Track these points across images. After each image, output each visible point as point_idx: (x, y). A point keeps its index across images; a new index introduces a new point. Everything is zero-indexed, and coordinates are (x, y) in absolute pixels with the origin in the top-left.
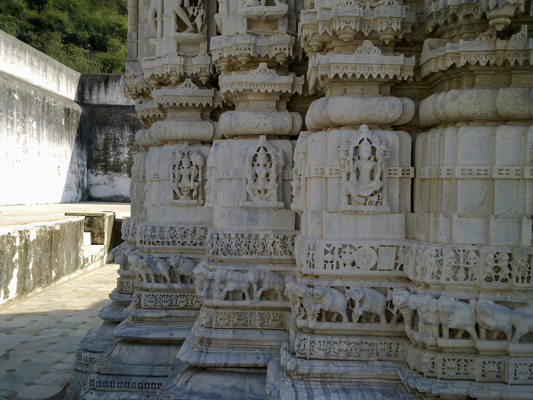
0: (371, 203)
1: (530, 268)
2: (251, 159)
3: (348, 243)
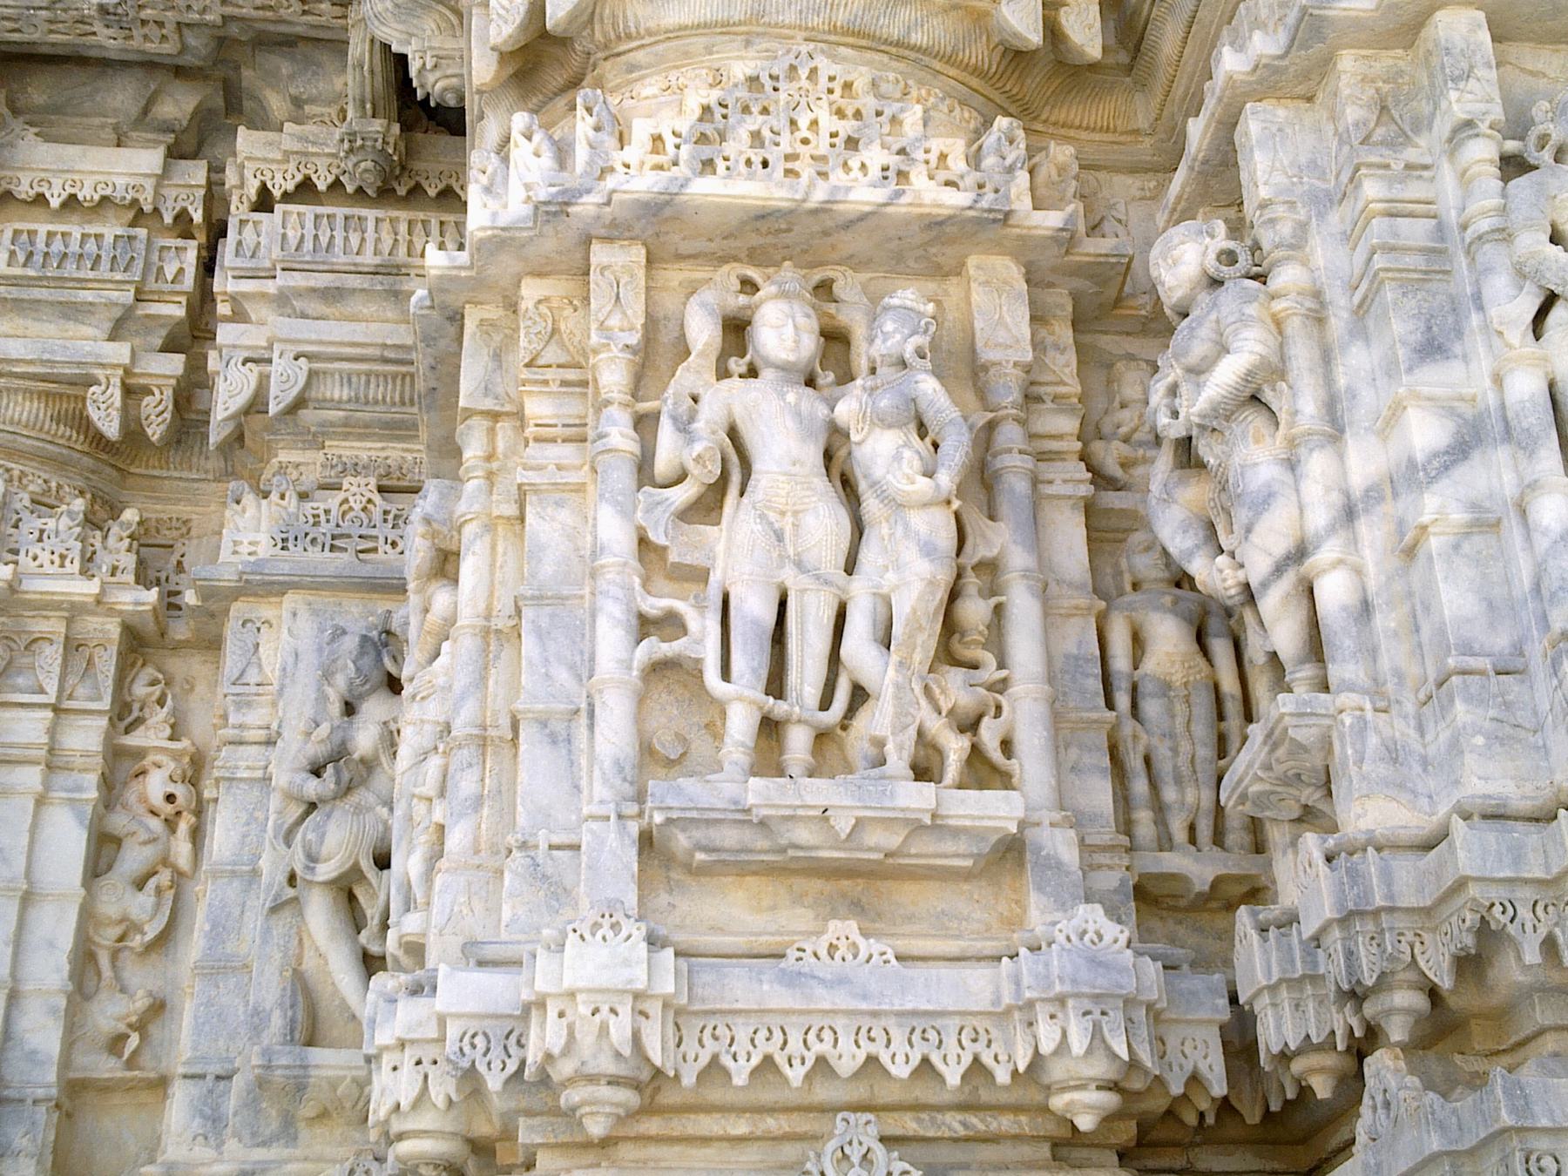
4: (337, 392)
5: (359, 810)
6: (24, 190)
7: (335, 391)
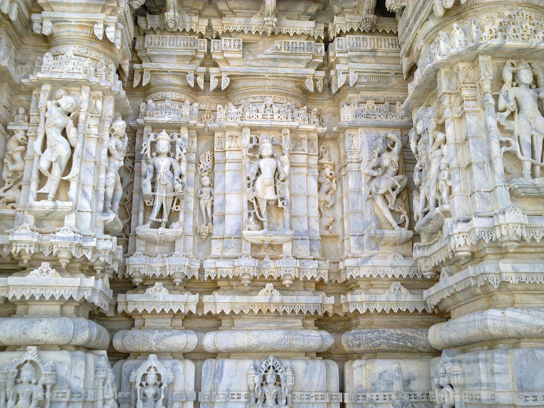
5: (387, 178)
6: (284, 32)
7: (364, 80)
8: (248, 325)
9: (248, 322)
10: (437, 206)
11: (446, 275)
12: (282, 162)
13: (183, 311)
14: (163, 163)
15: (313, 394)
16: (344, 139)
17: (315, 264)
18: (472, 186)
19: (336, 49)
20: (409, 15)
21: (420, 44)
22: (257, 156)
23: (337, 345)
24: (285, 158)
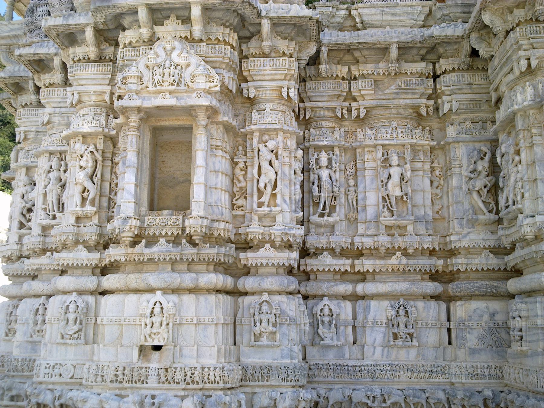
0: (74, 338)
1: (132, 375)
2: (35, 311)
3: (59, 362)
4: (463, 107)
5: (480, 179)
6: (403, 72)
8: (385, 279)
9: (384, 277)
10: (514, 204)
11: (519, 248)
12: (405, 169)
13: (342, 270)
14: (325, 173)
15: (430, 322)
16: (449, 149)
17: (430, 239)
18: (538, 194)
19: (443, 84)
20: (496, 64)
21: (503, 88)
22: (388, 165)
23: (445, 291)
24: (408, 166)
